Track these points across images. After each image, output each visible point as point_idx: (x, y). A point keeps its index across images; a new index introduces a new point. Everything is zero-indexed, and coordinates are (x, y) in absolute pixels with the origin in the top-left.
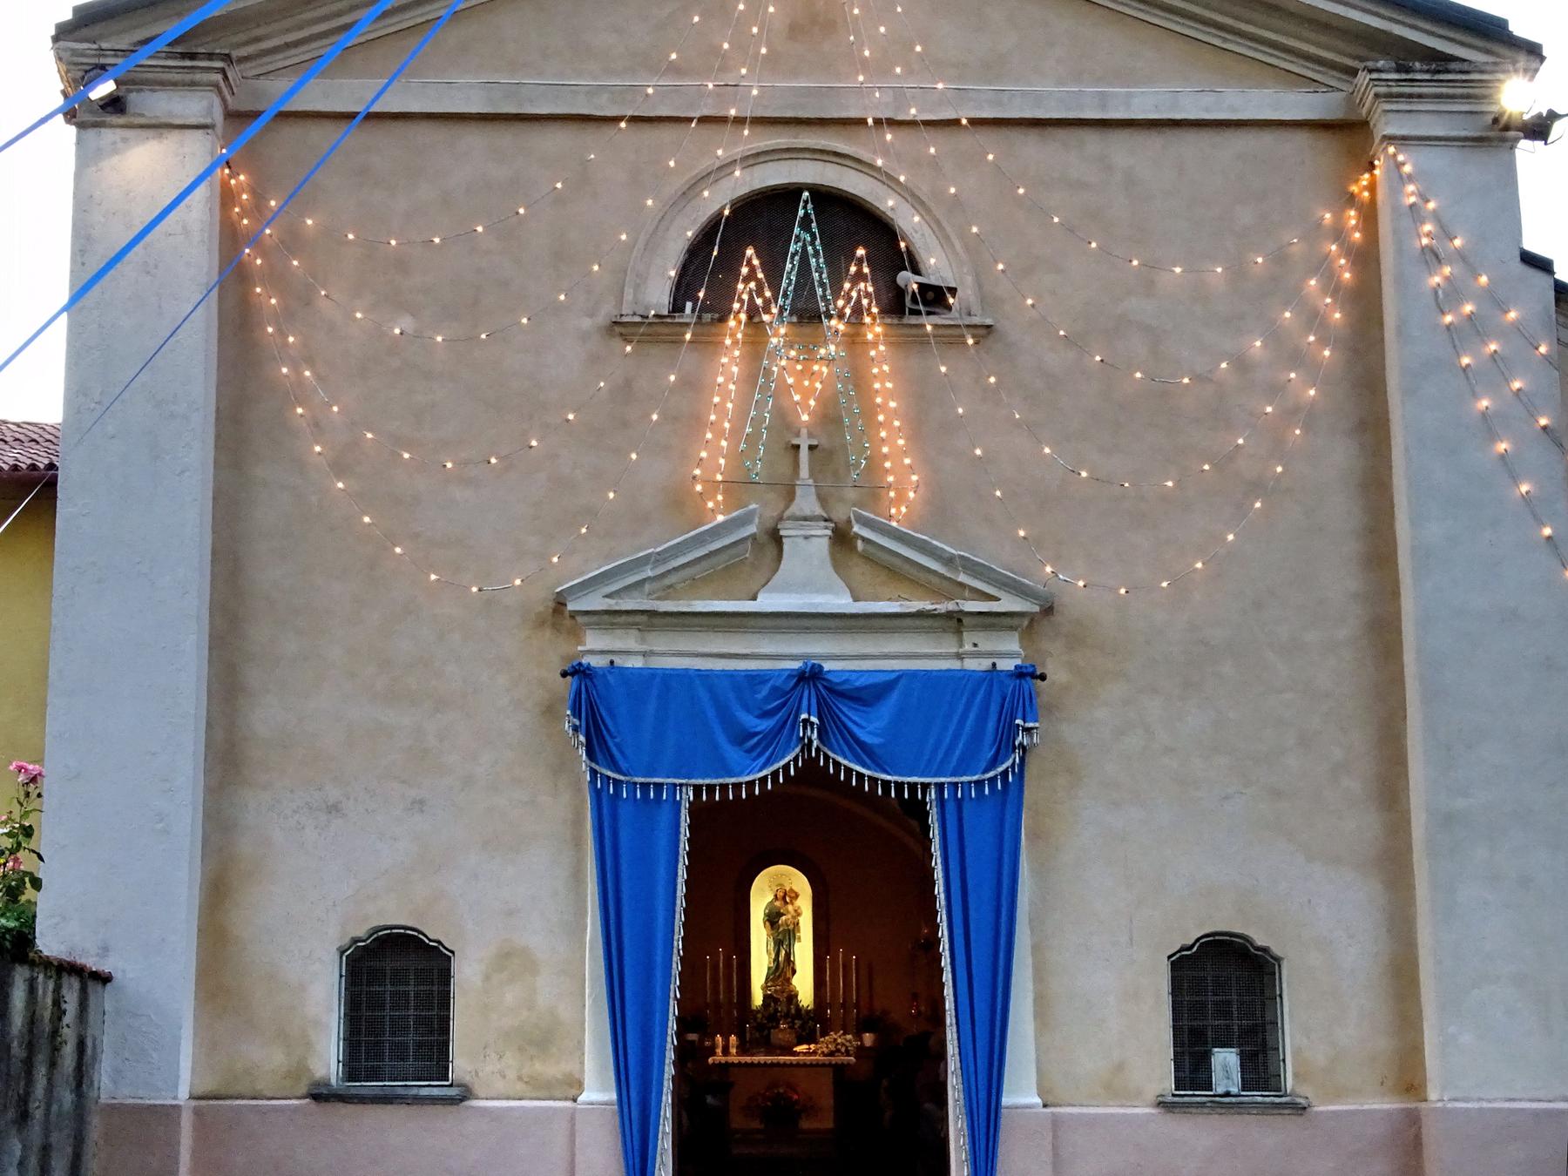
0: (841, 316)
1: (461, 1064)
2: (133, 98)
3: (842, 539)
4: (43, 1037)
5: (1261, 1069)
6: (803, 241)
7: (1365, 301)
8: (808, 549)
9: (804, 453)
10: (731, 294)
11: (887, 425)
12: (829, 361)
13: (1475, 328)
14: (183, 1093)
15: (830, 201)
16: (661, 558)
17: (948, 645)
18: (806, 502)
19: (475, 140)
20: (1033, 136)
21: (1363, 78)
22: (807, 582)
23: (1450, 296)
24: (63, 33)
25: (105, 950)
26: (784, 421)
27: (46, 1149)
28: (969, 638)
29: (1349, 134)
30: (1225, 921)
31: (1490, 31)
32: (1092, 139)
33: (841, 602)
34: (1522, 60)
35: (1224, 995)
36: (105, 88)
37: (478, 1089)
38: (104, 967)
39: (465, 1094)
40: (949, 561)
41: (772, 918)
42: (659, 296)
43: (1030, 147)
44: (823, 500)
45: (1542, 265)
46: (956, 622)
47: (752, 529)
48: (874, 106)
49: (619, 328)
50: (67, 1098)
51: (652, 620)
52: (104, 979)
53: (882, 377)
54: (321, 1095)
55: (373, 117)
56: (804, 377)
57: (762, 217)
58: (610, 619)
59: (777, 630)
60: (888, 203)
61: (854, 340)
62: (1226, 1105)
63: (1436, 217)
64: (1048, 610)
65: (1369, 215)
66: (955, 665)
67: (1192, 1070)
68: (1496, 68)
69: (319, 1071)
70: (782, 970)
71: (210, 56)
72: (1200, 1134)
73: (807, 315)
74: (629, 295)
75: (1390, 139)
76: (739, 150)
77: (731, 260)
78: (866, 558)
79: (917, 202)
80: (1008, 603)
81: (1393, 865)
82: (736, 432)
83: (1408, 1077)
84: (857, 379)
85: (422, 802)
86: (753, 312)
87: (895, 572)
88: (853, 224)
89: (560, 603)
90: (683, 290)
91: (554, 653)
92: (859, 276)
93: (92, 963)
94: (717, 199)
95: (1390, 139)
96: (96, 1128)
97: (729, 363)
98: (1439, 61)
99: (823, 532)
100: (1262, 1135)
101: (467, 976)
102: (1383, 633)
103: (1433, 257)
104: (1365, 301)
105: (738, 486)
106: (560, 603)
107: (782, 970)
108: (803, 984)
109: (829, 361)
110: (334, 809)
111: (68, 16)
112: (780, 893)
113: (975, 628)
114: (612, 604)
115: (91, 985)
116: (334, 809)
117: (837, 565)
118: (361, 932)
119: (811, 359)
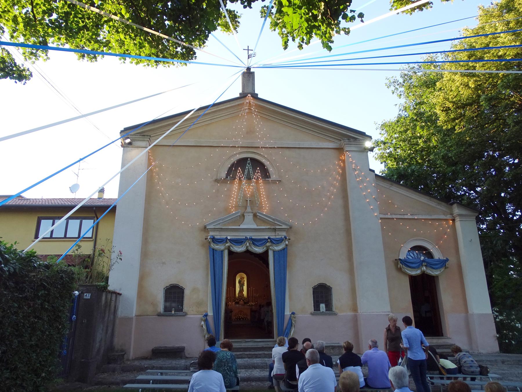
0: (255, 179)
1: (185, 309)
2: (134, 143)
3: (255, 216)
4: (108, 305)
5: (329, 307)
6: (249, 166)
7: (343, 176)
8: (249, 217)
9: (248, 201)
10: (236, 175)
11: (263, 197)
12: (252, 186)
13: (362, 181)
14: (134, 315)
15: (253, 160)
16: (223, 219)
17: (273, 234)
18: (249, 209)
19: (193, 150)
20: (288, 149)
21: (342, 141)
22: (249, 223)
23: (358, 176)
24: (122, 132)
25: (120, 289)
26: (245, 196)
27: (107, 327)
28: (277, 232)
29: (340, 150)
30: (322, 281)
31: (363, 134)
32: (297, 150)
33: (255, 226)
34: (369, 138)
35: (322, 294)
36: (128, 141)
37: (189, 313)
38: (120, 292)
39: (186, 314)
40: (274, 219)
41: (240, 282)
42: (223, 175)
43: (287, 152)
44: (252, 209)
45: (373, 171)
46: (275, 230)
47: (239, 214)
48: (261, 144)
49: (217, 181)
50: (112, 317)
51: (221, 230)
52: (120, 294)
53: (262, 189)
54: (159, 315)
55: (173, 146)
56: (248, 188)
57: (241, 163)
58: (214, 230)
59: (244, 231)
60: (263, 161)
61: (257, 182)
62: (323, 314)
63: (355, 163)
64: (291, 228)
65: (344, 161)
66: (275, 237)
67: (317, 307)
68: (364, 140)
69: (159, 311)
70: (241, 291)
71: (147, 136)
72: (319, 319)
73: (249, 178)
74: (219, 175)
75: (347, 151)
76: (238, 152)
77: (236, 169)
78: (259, 219)
79: (268, 160)
80: (284, 227)
81: (351, 272)
82: (236, 198)
83: (355, 309)
84: (258, 189)
85: (180, 262)
86: (240, 178)
87: (264, 221)
88: (257, 163)
89: (205, 227)
90: (228, 174)
91: (204, 235)
92: (258, 172)
93: (118, 291)
94: (234, 160)
95: (347, 151)
96: (117, 321)
97: (236, 186)
98: (355, 139)
99: (251, 215)
100: (329, 319)
101: (187, 292)
102: (348, 232)
103: (355, 170)
104: (343, 176)
105: (237, 207)
106: (205, 227)
107: (241, 291)
108: (245, 293)
109: (252, 186)
110: (164, 263)
111: (123, 129)
112: (241, 279)
113: (278, 231)
114: (213, 227)
115: (118, 296)
116: (164, 263)
117: (254, 220)
118: (168, 285)
119: (249, 186)
